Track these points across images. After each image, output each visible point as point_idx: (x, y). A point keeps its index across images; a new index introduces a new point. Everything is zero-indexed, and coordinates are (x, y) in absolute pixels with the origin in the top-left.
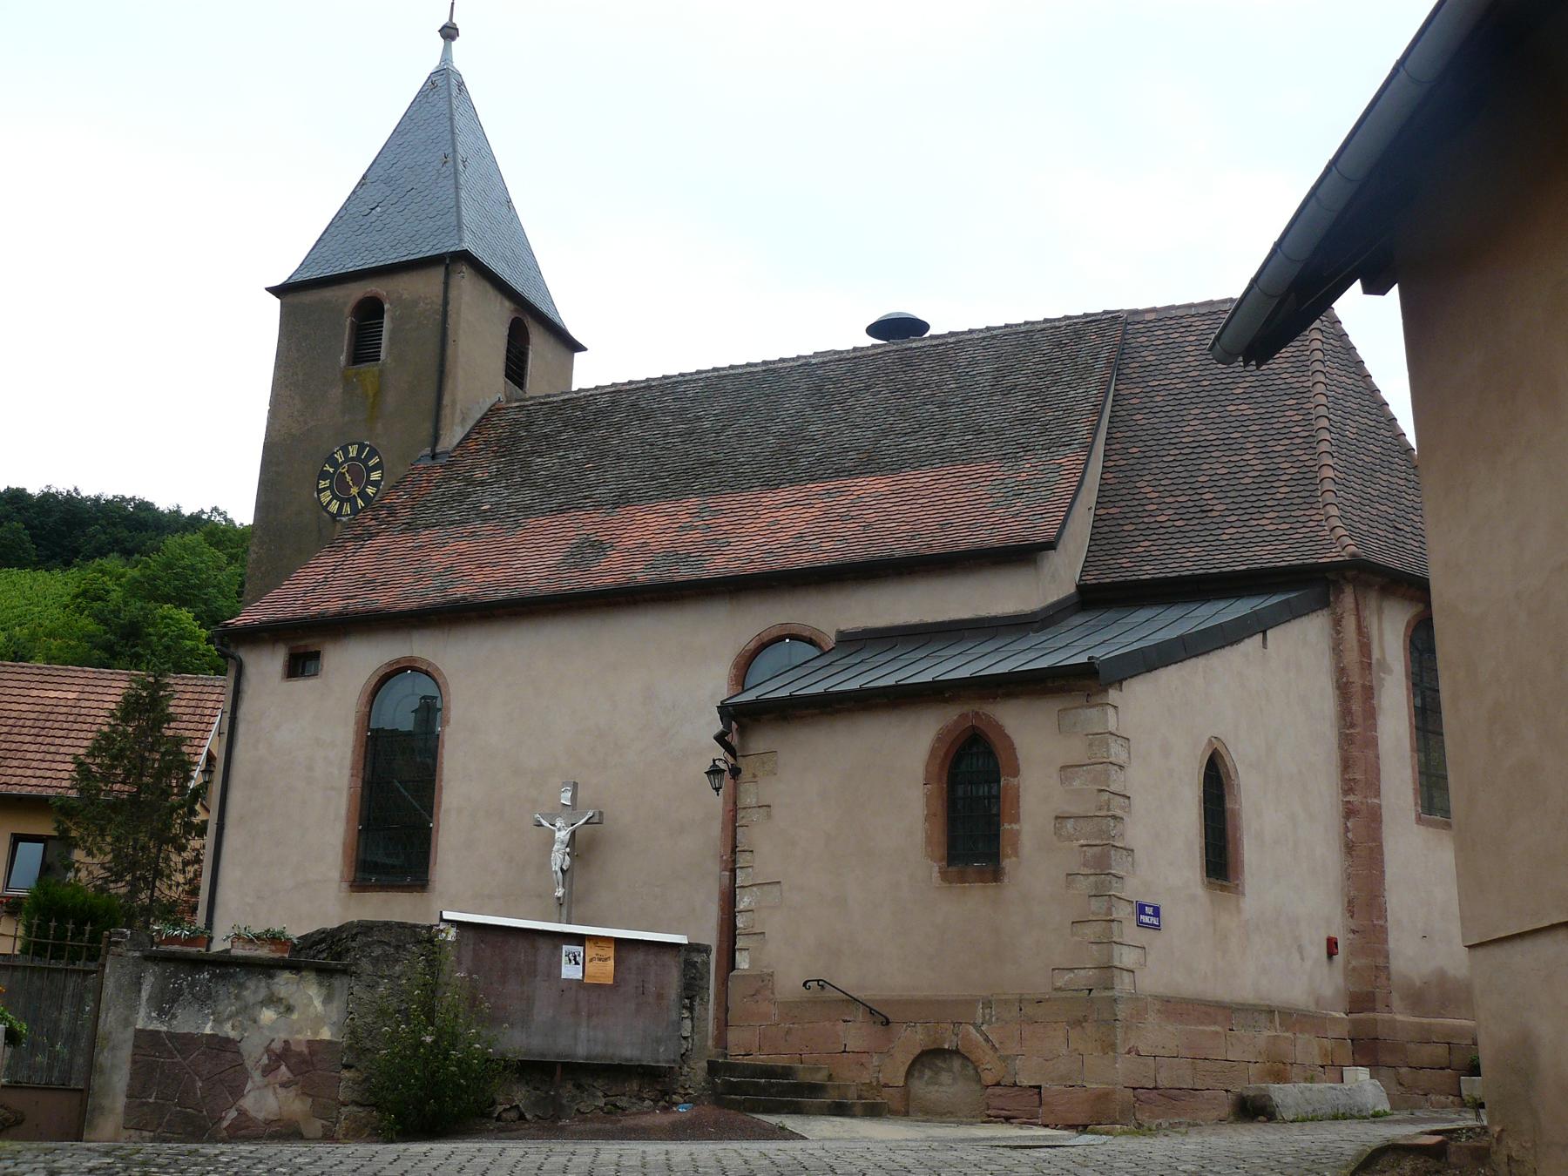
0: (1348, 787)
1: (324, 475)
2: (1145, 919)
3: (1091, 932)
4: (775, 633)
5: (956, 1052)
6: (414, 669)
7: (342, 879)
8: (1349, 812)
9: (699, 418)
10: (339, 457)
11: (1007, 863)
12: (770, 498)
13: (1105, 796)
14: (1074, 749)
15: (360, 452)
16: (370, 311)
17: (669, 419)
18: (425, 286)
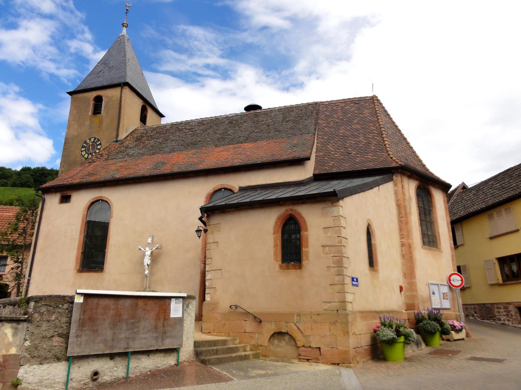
0: (402, 237)
1: (83, 147)
2: (354, 283)
3: (337, 288)
4: (219, 187)
5: (287, 333)
6: (102, 200)
7: (75, 269)
8: (403, 245)
9: (196, 130)
10: (88, 141)
11: (304, 262)
12: (218, 149)
13: (340, 238)
14: (329, 222)
15: (94, 140)
16: (98, 100)
17: (187, 131)
18: (115, 93)
